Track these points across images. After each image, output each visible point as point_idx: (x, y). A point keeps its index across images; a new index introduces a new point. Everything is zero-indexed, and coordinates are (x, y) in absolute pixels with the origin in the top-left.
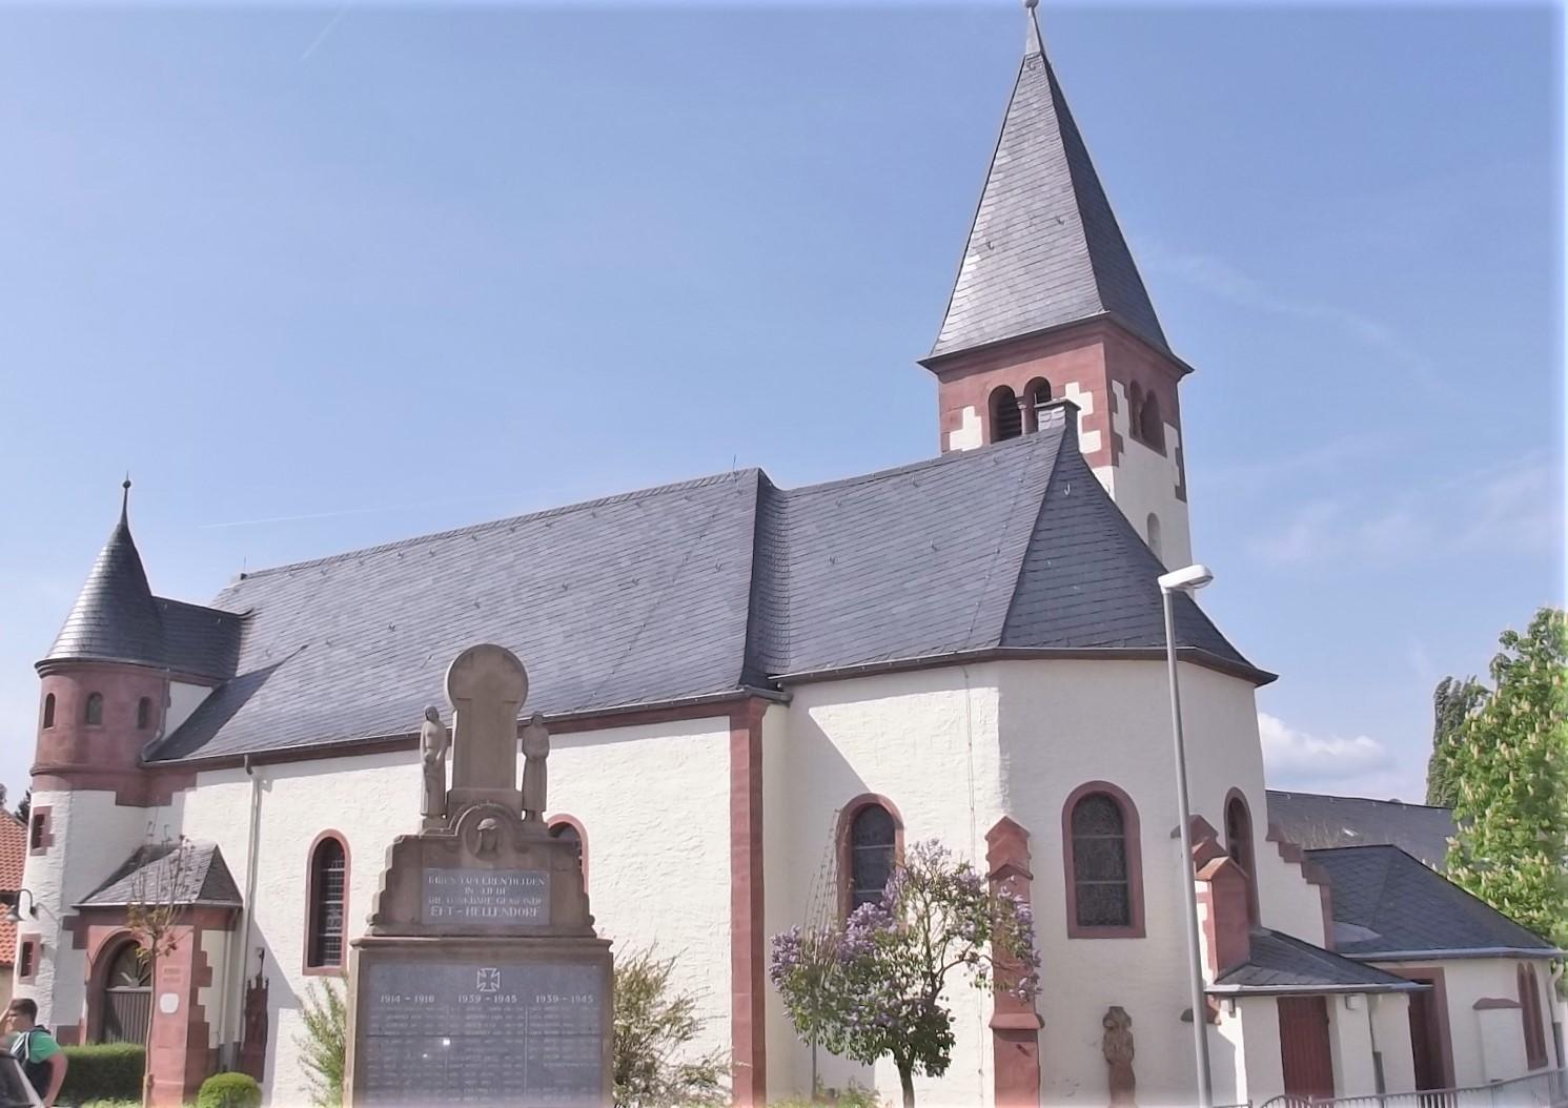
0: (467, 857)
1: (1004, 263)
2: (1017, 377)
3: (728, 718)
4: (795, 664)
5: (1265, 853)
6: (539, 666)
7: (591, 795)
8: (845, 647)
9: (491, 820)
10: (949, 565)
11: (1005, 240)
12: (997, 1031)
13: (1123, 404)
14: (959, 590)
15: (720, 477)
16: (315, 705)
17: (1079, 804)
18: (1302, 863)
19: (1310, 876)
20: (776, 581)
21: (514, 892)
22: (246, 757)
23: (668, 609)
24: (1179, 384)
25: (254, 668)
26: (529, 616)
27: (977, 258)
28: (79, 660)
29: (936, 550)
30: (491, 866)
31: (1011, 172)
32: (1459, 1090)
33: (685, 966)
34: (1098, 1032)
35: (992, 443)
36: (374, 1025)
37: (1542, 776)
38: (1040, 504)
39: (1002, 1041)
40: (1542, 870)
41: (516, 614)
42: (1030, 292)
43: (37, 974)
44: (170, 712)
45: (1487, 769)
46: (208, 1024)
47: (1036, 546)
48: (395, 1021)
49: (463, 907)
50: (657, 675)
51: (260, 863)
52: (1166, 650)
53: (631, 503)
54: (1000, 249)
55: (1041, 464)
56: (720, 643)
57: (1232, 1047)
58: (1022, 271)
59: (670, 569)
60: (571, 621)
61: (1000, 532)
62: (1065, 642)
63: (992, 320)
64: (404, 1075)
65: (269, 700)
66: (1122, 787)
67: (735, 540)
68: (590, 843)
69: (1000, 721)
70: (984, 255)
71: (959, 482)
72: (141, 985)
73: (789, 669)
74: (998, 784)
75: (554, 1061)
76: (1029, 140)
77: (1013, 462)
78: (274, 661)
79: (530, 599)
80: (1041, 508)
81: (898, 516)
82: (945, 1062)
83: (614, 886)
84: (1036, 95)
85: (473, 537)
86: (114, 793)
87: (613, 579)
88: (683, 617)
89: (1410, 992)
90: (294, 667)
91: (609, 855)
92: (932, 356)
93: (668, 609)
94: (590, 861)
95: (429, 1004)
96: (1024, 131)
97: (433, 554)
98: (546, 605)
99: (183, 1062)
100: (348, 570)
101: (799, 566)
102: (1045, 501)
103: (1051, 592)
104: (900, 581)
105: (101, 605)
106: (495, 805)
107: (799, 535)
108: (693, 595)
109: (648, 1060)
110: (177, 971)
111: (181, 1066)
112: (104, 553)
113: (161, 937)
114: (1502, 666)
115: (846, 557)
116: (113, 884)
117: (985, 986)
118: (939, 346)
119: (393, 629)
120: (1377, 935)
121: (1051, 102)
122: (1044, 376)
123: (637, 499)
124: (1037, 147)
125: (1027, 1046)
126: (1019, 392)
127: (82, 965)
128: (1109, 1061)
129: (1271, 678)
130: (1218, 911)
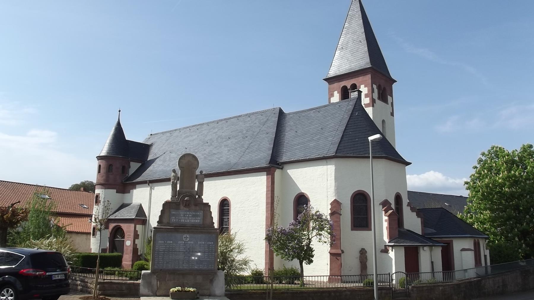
0: (182, 207)
2: (348, 83)
3: (266, 172)
5: (406, 210)
6: (221, 159)
11: (346, 47)
12: (331, 254)
13: (376, 91)
14: (327, 140)
17: (355, 196)
18: (416, 212)
19: (418, 215)
22: (148, 181)
23: (254, 144)
24: (393, 85)
25: (152, 158)
26: (220, 145)
27: (339, 52)
28: (106, 156)
30: (188, 209)
31: (349, 28)
32: (435, 272)
33: (254, 236)
34: (358, 255)
36: (157, 248)
37: (488, 190)
39: (331, 256)
40: (488, 215)
42: (352, 61)
43: (96, 235)
45: (475, 188)
46: (138, 249)
47: (347, 128)
48: (162, 247)
49: (180, 219)
50: (249, 161)
51: (151, 208)
52: (370, 156)
53: (247, 116)
54: (345, 49)
57: (392, 259)
58: (351, 55)
59: (255, 133)
60: (230, 147)
61: (338, 125)
63: (342, 68)
64: (164, 261)
65: (155, 166)
66: (367, 192)
69: (335, 174)
71: (330, 111)
72: (122, 238)
73: (283, 160)
74: (334, 190)
75: (203, 258)
76: (354, 20)
78: (158, 156)
79: (221, 141)
84: (356, 8)
85: (208, 125)
86: (115, 190)
87: (241, 136)
88: (257, 146)
89: (442, 246)
90: (162, 158)
91: (236, 207)
92: (327, 78)
93: (254, 144)
94: (231, 209)
96: (352, 18)
97: (198, 129)
98: (224, 143)
99: (132, 257)
103: (350, 140)
104: (312, 137)
105: (113, 142)
106: (189, 194)
111: (131, 259)
112: (114, 129)
116: (115, 213)
118: (328, 75)
119: (186, 148)
120: (436, 231)
121: (360, 10)
123: (249, 115)
125: (338, 258)
126: (349, 87)
128: (361, 262)
129: (409, 164)
130: (390, 224)
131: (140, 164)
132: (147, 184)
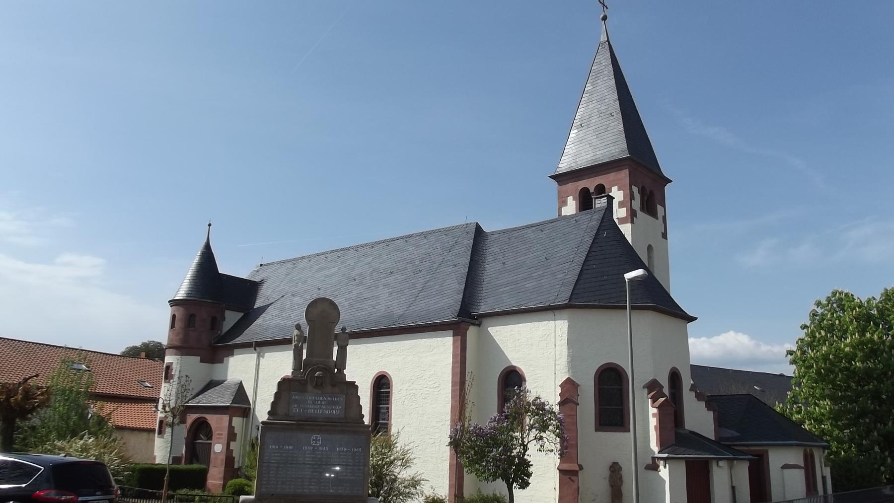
0: (310, 387)
1: (588, 133)
2: (591, 184)
4: (484, 308)
5: (689, 397)
6: (377, 307)
7: (395, 363)
8: (505, 301)
9: (321, 372)
10: (552, 266)
11: (588, 123)
13: (637, 196)
14: (555, 277)
15: (460, 226)
16: (284, 322)
19: (709, 407)
20: (479, 272)
21: (329, 403)
22: (254, 343)
24: (665, 187)
27: (576, 131)
29: (547, 259)
30: (320, 392)
31: (592, 93)
34: (607, 473)
35: (580, 211)
38: (592, 240)
41: (370, 284)
43: (165, 434)
44: (225, 323)
47: (589, 258)
55: (595, 222)
56: (452, 298)
57: (664, 481)
58: (595, 137)
59: (435, 266)
62: (598, 301)
63: (581, 159)
64: (278, 479)
67: (464, 253)
68: (393, 384)
70: (579, 130)
72: (207, 440)
73: (480, 310)
74: (566, 363)
77: (583, 221)
80: (593, 242)
81: (533, 244)
82: (528, 484)
83: (403, 403)
84: (604, 60)
86: (199, 357)
89: (749, 460)
95: (290, 450)
97: (339, 257)
98: (383, 280)
99: (223, 474)
100: (302, 264)
101: (490, 265)
102: (594, 239)
104: (531, 273)
107: (492, 250)
108: (443, 277)
109: (393, 477)
110: (221, 434)
111: (222, 475)
112: (199, 254)
113: (176, 418)
114: (814, 314)
115: (510, 262)
117: (544, 451)
120: (739, 434)
122: (604, 184)
123: (425, 235)
124: (604, 82)
125: (573, 478)
126: (592, 190)
127: (183, 431)
128: (612, 486)
131: (241, 314)
132: (253, 349)
